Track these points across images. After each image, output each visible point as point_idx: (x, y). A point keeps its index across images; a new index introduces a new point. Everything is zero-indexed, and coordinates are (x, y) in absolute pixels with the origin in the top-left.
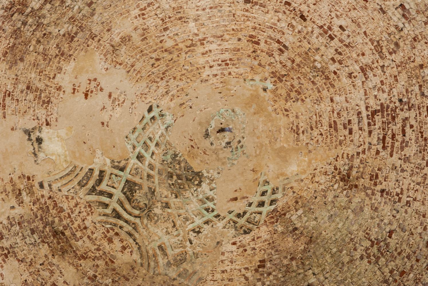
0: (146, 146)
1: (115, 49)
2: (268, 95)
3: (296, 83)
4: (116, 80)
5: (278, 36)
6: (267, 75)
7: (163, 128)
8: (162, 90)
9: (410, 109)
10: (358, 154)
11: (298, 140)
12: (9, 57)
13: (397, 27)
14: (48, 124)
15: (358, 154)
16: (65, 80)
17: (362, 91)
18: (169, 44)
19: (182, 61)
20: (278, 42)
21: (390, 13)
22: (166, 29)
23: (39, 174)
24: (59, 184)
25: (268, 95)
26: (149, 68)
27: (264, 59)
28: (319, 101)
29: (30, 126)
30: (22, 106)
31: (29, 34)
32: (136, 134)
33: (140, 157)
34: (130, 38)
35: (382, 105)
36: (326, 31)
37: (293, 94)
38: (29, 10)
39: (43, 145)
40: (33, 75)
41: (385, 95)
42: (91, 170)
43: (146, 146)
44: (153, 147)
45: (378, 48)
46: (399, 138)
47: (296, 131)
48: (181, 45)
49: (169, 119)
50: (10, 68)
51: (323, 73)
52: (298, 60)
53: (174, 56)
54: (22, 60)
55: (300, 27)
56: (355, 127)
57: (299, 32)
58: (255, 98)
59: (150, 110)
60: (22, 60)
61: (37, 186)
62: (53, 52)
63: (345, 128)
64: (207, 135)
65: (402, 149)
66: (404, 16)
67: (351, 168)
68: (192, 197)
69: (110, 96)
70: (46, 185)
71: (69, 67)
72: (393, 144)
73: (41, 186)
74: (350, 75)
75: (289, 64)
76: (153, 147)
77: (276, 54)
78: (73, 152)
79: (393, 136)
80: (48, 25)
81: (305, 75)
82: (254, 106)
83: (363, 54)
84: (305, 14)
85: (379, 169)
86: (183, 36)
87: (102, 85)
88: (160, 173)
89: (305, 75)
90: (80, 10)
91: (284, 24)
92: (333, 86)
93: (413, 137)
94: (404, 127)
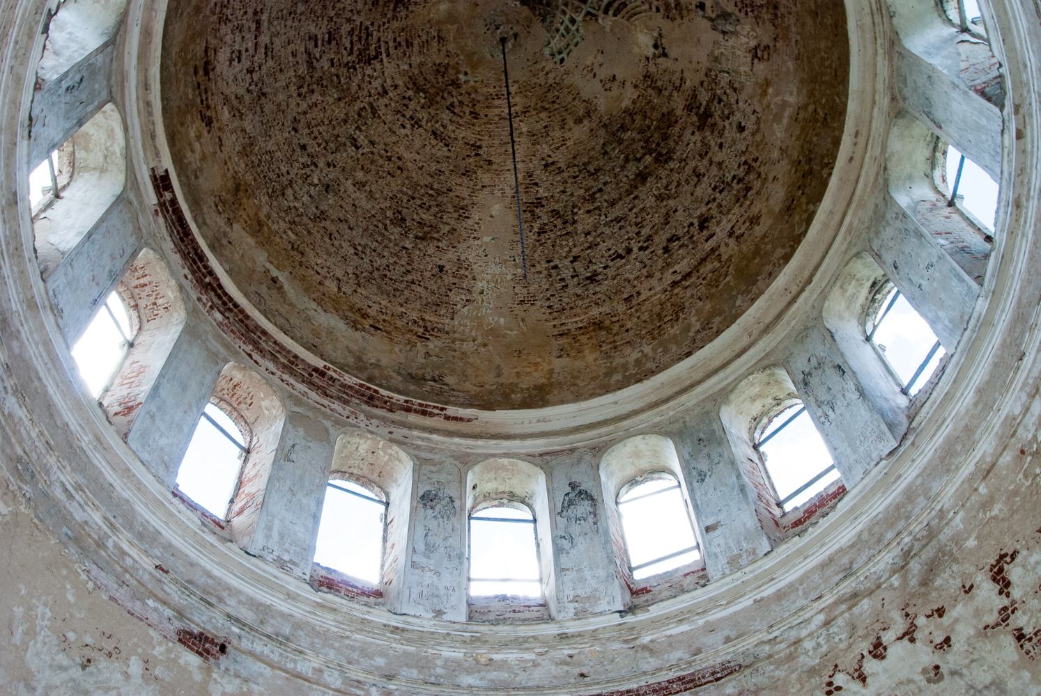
0: (567, 30)
1: (588, 114)
2: (463, 69)
3: (440, 79)
4: (590, 88)
5: (455, 118)
6: (464, 86)
7: (552, 44)
8: (551, 76)
9: (348, 63)
10: (389, 22)
11: (439, 31)
12: (673, 119)
13: (361, 130)
14: (648, 58)
15: (389, 22)
16: (630, 94)
17: (386, 74)
18: (543, 115)
19: (534, 100)
20: (454, 113)
21: (366, 142)
22: (546, 127)
23: (659, 20)
24: (643, 8)
25: (463, 69)
26: (561, 96)
27: (466, 100)
28: (421, 64)
29: (662, 60)
30: (667, 78)
31: (656, 135)
32: (575, 41)
33: (573, 21)
34: (575, 123)
35: (370, 64)
36: (417, 123)
37: (442, 69)
38: (654, 155)
39: (652, 42)
40: (655, 101)
41: (367, 72)
42: (615, 15)
43: (567, 30)
44: (562, 29)
45: (374, 111)
46: (355, 38)
47: (441, 39)
48: (534, 113)
49: (547, 51)
50: (673, 110)
51: (418, 89)
52: (438, 99)
53: (539, 104)
54: (663, 115)
55: (437, 126)
56: (391, 44)
57: (437, 122)
58: (474, 66)
59: (562, 60)
60: (663, 115)
61: (662, 10)
62: (638, 118)
63: (400, 43)
64: (516, 36)
65: (353, 29)
66: (355, 140)
67: (395, 9)
68: (669, 278)
69: (595, 75)
70: (654, 9)
71: (626, 103)
72: (360, 32)
73: (658, 10)
74: (396, 87)
75: (446, 95)
76: (562, 29)
77: (457, 103)
78: (629, 32)
79: (360, 40)
80: (640, 140)
81: (433, 86)
82: (475, 60)
83: (386, 106)
84: (432, 137)
85: (371, 10)
86: (532, 120)
87: (600, 85)
88: (557, 7)
89: (433, 86)
90: (614, 149)
91: (450, 128)
92: (410, 77)
93: (344, 40)
94: (352, 48)
